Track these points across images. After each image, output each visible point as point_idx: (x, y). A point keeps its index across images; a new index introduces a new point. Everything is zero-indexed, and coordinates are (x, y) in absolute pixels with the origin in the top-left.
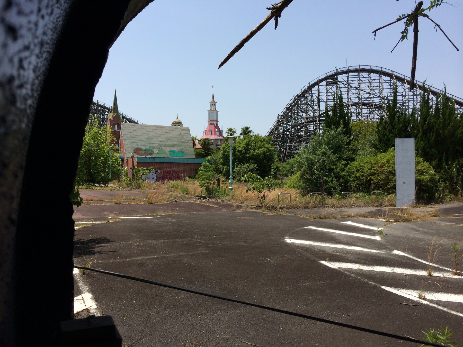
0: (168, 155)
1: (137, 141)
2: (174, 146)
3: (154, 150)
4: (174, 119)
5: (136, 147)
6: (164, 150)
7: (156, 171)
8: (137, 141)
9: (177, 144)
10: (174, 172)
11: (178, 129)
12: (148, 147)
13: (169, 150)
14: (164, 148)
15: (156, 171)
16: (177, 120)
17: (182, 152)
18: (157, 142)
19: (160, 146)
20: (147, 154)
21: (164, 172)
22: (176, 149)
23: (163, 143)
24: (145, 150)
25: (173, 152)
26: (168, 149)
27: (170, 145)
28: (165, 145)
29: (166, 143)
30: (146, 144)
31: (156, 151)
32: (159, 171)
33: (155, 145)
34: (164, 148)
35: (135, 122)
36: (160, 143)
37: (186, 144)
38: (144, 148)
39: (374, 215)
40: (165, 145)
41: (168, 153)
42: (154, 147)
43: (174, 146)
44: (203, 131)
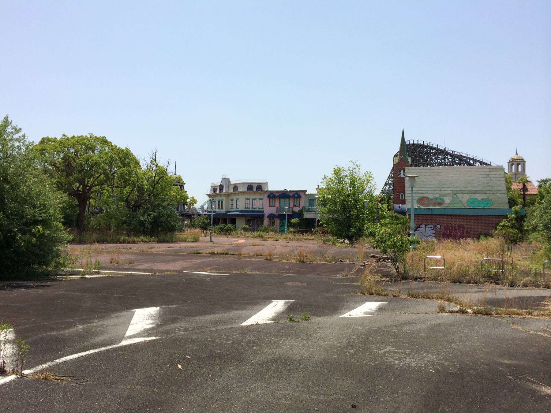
0: (466, 205)
1: (423, 189)
2: (475, 192)
3: (445, 198)
4: (513, 156)
5: (421, 196)
6: (460, 198)
7: (435, 227)
8: (423, 189)
9: (482, 189)
10: (461, 227)
11: (485, 170)
12: (437, 196)
13: (468, 198)
14: (460, 195)
15: (435, 227)
16: (516, 157)
17: (487, 200)
18: (451, 189)
19: (455, 193)
20: (435, 204)
21: (447, 227)
22: (478, 196)
23: (458, 189)
24: (432, 200)
25: (474, 201)
26: (467, 197)
27: (469, 192)
28: (463, 192)
29: (464, 189)
30: (435, 192)
31: (447, 201)
32: (439, 226)
33: (447, 192)
34: (460, 195)
35: (487, 164)
36: (455, 189)
37: (495, 189)
38: (431, 196)
39: (406, 324)
40: (463, 192)
41: (465, 202)
42: (445, 195)
43: (475, 192)
44: (185, 180)
